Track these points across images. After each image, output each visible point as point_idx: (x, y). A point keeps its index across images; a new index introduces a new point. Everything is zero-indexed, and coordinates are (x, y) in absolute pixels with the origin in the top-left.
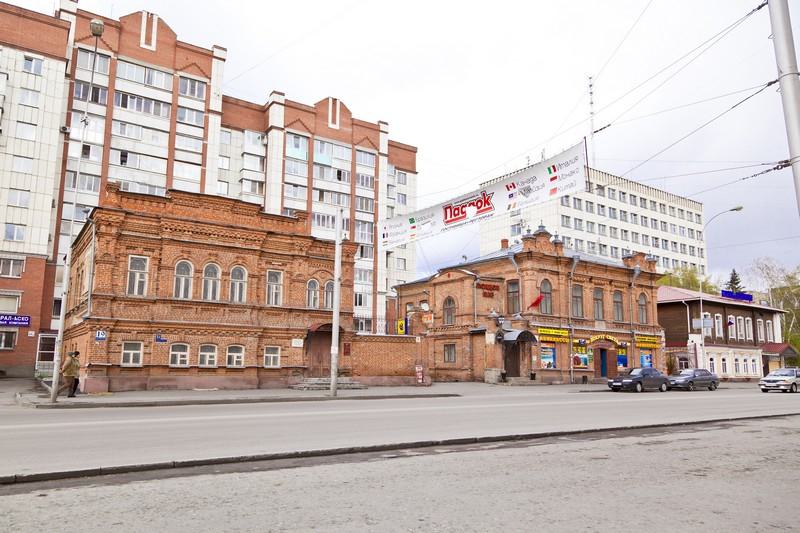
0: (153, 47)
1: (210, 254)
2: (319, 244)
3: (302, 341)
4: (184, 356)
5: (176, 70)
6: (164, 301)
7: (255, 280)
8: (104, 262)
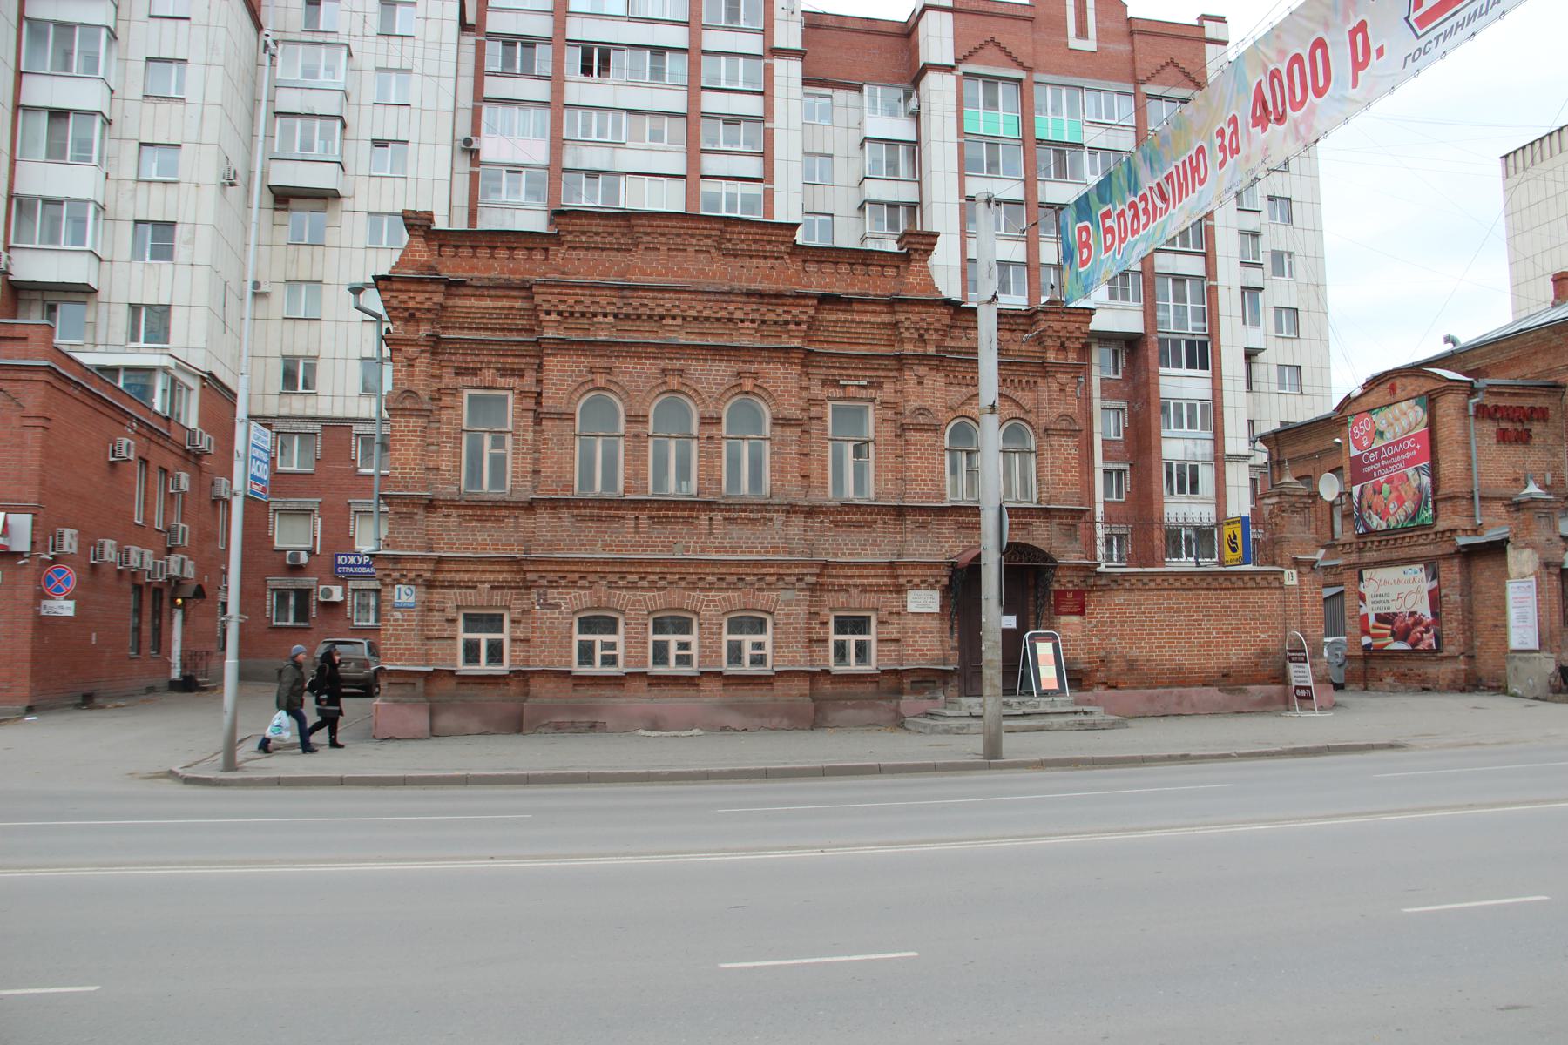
1: (664, 372)
4: (759, 646)
5: (1137, 83)
6: (553, 504)
7: (793, 433)
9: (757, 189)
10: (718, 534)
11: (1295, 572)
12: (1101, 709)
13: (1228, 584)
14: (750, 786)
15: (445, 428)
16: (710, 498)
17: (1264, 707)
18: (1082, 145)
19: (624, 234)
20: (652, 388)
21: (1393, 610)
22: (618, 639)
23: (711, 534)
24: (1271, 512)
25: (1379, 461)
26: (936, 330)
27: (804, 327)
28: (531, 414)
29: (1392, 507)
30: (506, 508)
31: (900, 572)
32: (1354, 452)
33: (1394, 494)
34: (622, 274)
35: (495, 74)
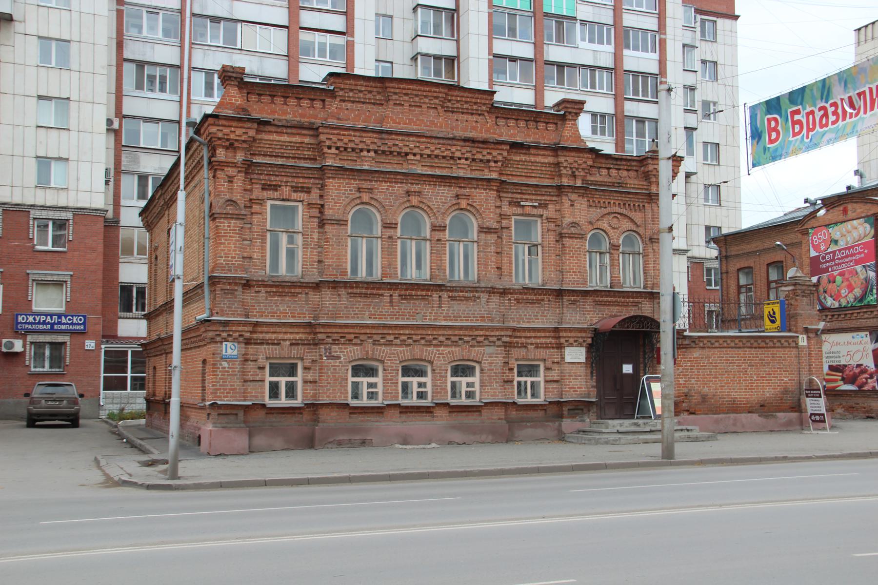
1: (408, 193)
2: (603, 163)
3: (583, 350)
6: (335, 285)
8: (228, 216)
9: (340, 40)
10: (445, 307)
11: (805, 337)
12: (697, 428)
13: (763, 344)
14: (652, 472)
15: (255, 228)
16: (440, 282)
17: (787, 427)
18: (575, 19)
19: (379, 93)
20: (403, 203)
21: (843, 362)
22: (378, 380)
23: (440, 307)
24: (787, 296)
25: (834, 260)
26: (583, 169)
27: (500, 164)
28: (316, 220)
29: (844, 292)
30: (300, 287)
31: (561, 334)
32: (813, 253)
33: (845, 283)
34: (381, 121)
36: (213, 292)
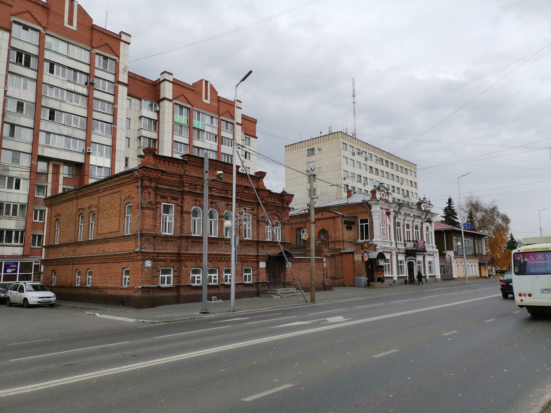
0: (74, 28)
3: (265, 263)
4: (215, 277)
5: (93, 48)
8: (148, 208)
18: (204, 131)
35: (13, 63)
36: (141, 239)
